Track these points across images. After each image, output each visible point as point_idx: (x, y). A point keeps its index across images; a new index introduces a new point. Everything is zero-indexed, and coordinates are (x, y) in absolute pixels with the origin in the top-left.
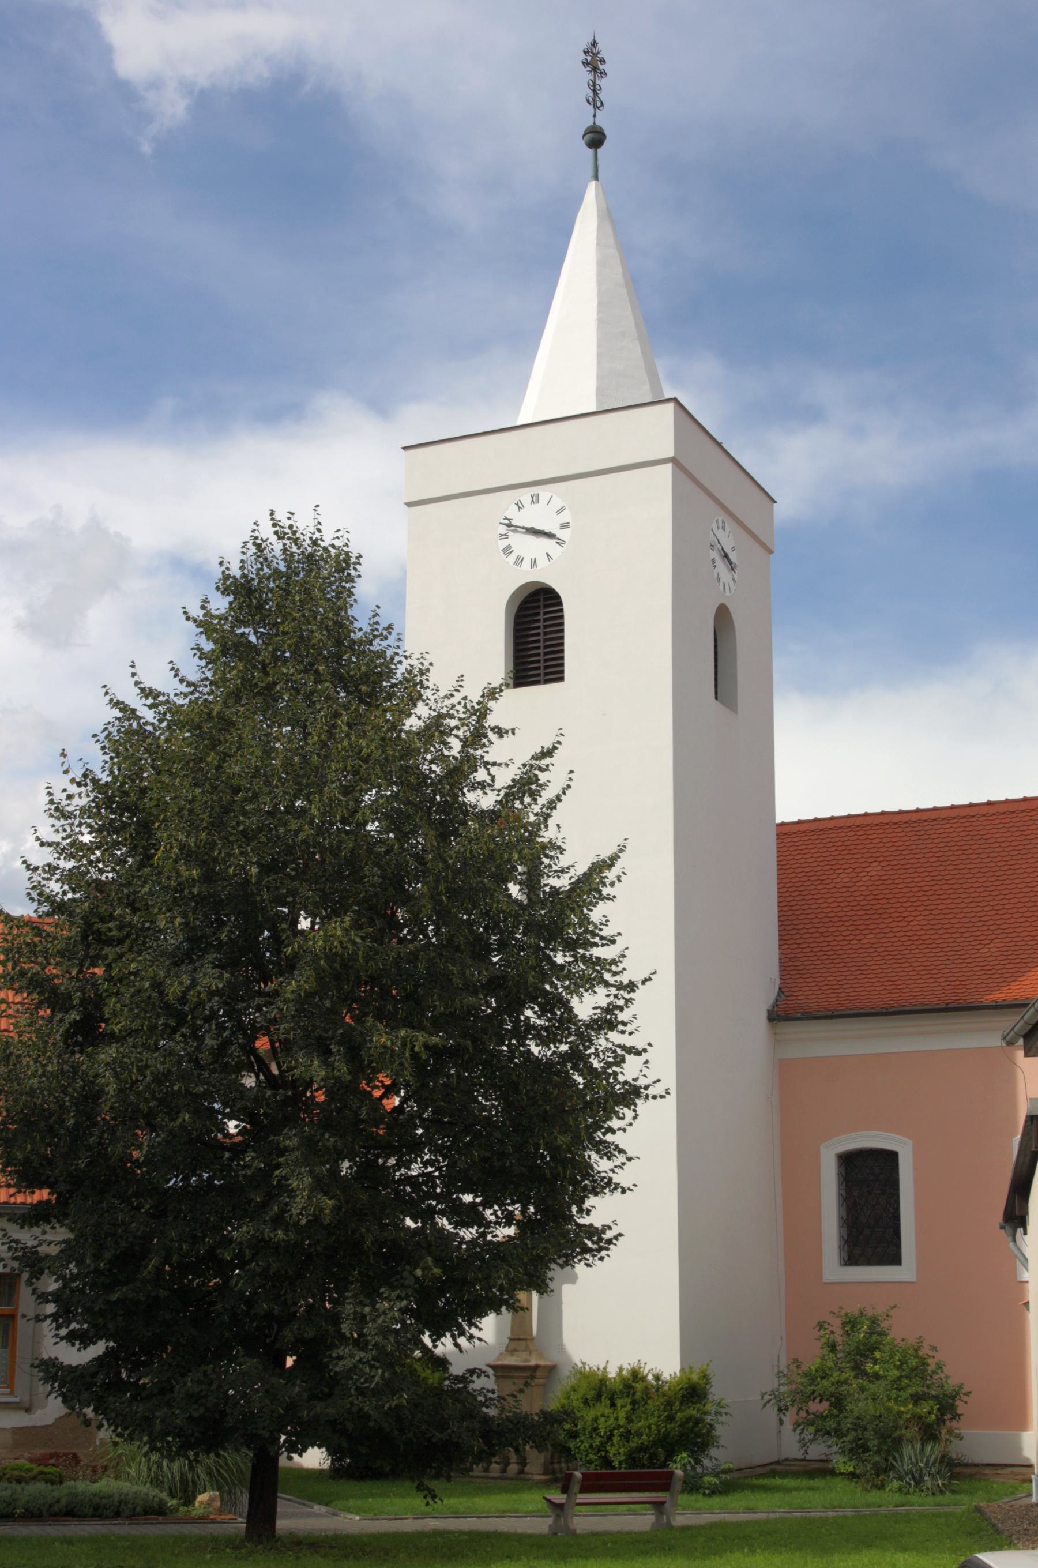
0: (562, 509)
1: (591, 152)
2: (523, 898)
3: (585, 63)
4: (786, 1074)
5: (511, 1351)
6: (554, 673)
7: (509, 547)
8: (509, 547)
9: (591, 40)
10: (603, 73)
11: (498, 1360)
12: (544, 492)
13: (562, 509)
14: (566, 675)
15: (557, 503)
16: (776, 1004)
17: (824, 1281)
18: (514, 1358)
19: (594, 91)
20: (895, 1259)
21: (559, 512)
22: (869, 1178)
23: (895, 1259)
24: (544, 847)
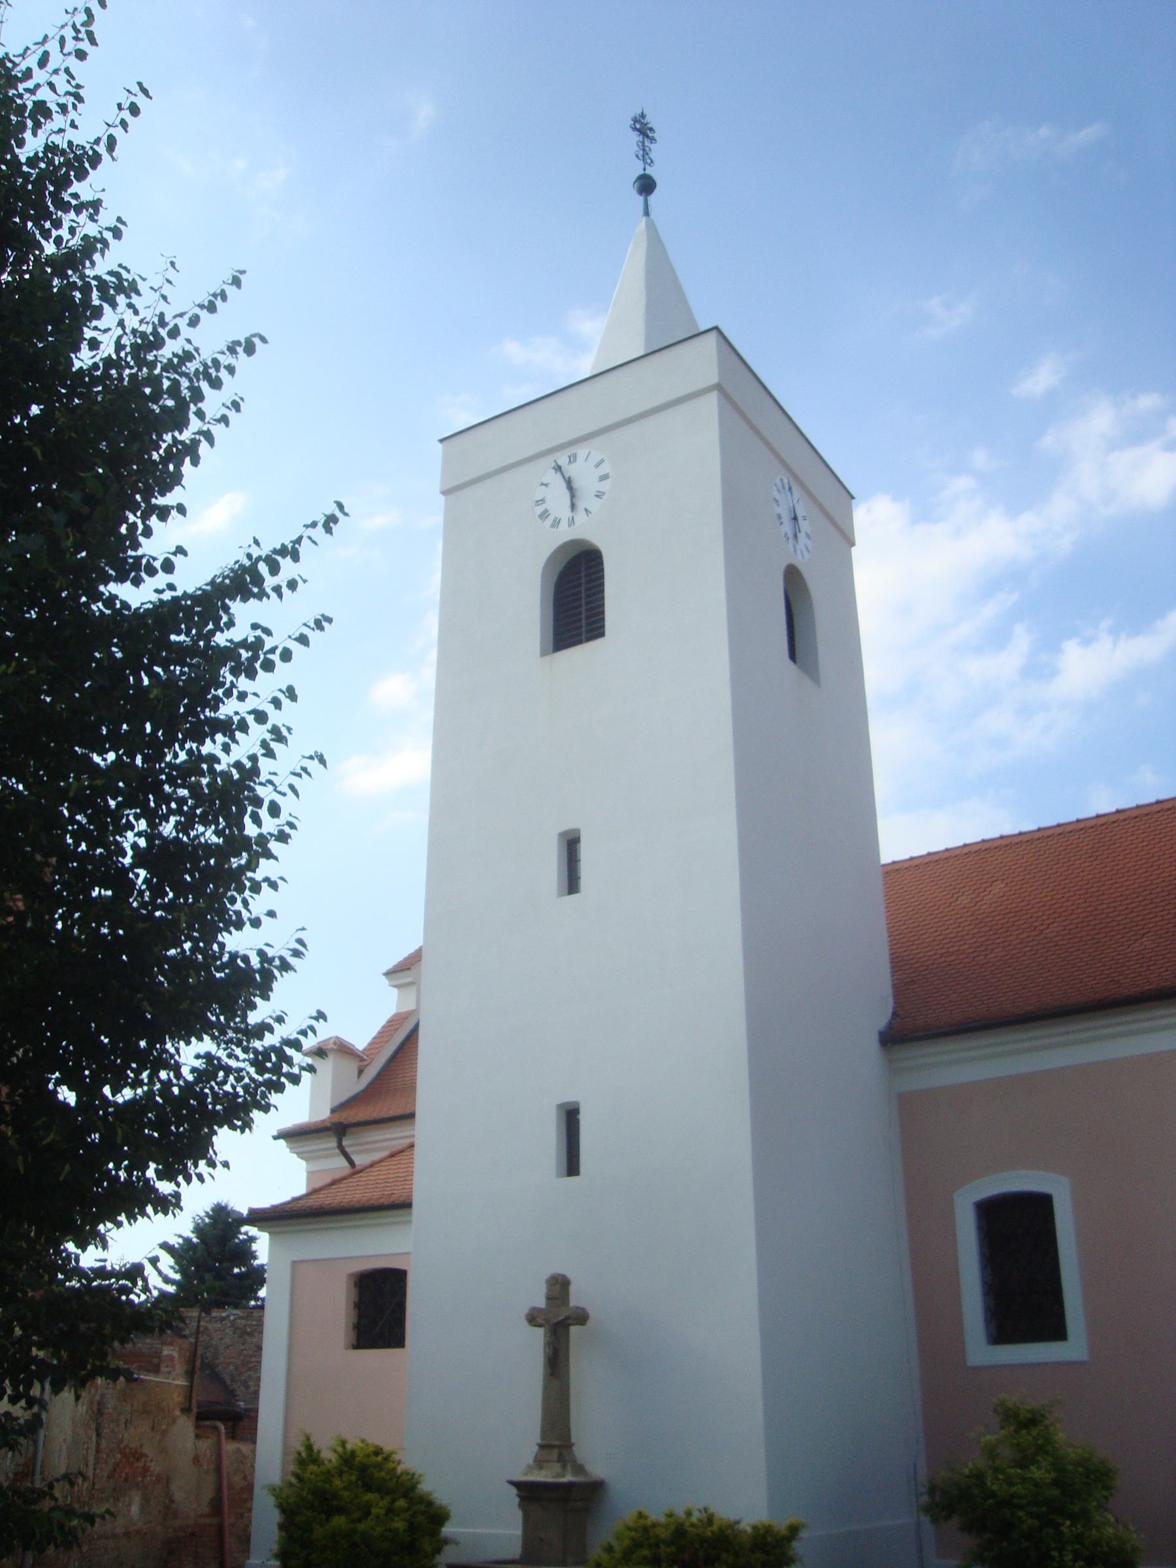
0: (602, 461)
1: (641, 198)
2: (103, 781)
3: (635, 129)
4: (911, 1111)
5: (539, 1463)
6: (595, 629)
7: (546, 511)
8: (546, 511)
9: (640, 112)
10: (652, 140)
11: (526, 1474)
12: (582, 452)
13: (602, 461)
14: (607, 633)
15: (596, 456)
16: (890, 1025)
17: (969, 1364)
18: (544, 1472)
19: (644, 150)
20: (1058, 1332)
21: (597, 466)
22: (1018, 1236)
23: (1058, 1332)
24: (229, 654)
